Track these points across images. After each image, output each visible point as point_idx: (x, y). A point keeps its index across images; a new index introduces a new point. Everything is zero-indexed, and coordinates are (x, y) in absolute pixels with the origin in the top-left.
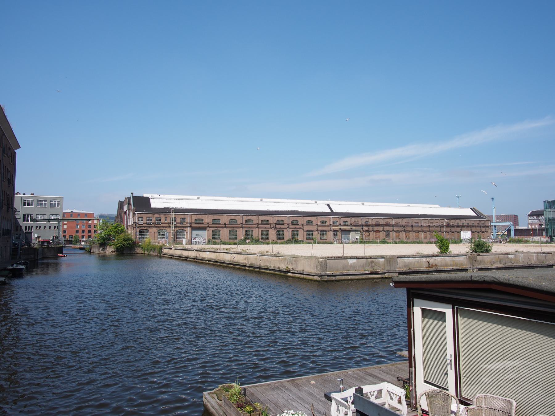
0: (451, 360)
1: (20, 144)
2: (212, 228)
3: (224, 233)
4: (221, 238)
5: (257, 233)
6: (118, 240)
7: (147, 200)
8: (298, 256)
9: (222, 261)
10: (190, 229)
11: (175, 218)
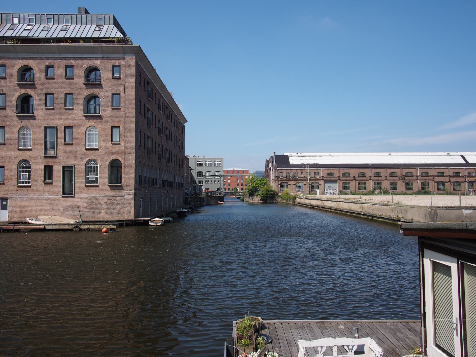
0: (457, 325)
1: (186, 119)
2: (342, 180)
3: (354, 185)
4: (351, 189)
5: (385, 185)
6: (262, 191)
7: (287, 157)
8: (407, 205)
9: (341, 209)
10: (323, 181)
11: (310, 172)
